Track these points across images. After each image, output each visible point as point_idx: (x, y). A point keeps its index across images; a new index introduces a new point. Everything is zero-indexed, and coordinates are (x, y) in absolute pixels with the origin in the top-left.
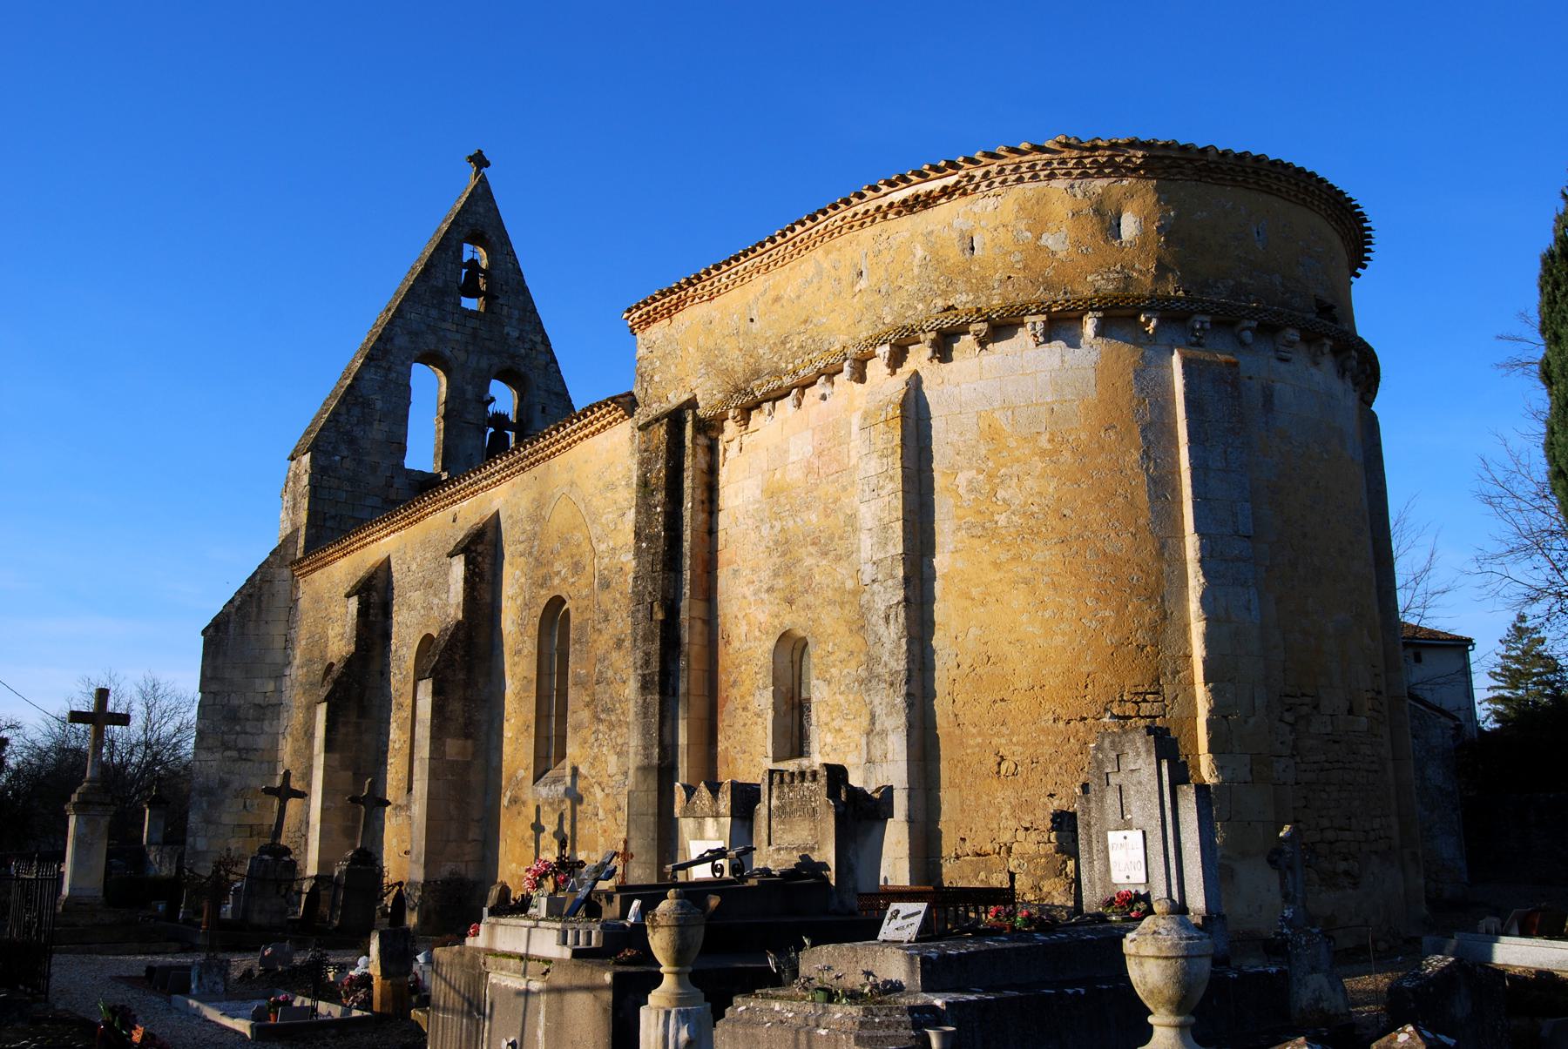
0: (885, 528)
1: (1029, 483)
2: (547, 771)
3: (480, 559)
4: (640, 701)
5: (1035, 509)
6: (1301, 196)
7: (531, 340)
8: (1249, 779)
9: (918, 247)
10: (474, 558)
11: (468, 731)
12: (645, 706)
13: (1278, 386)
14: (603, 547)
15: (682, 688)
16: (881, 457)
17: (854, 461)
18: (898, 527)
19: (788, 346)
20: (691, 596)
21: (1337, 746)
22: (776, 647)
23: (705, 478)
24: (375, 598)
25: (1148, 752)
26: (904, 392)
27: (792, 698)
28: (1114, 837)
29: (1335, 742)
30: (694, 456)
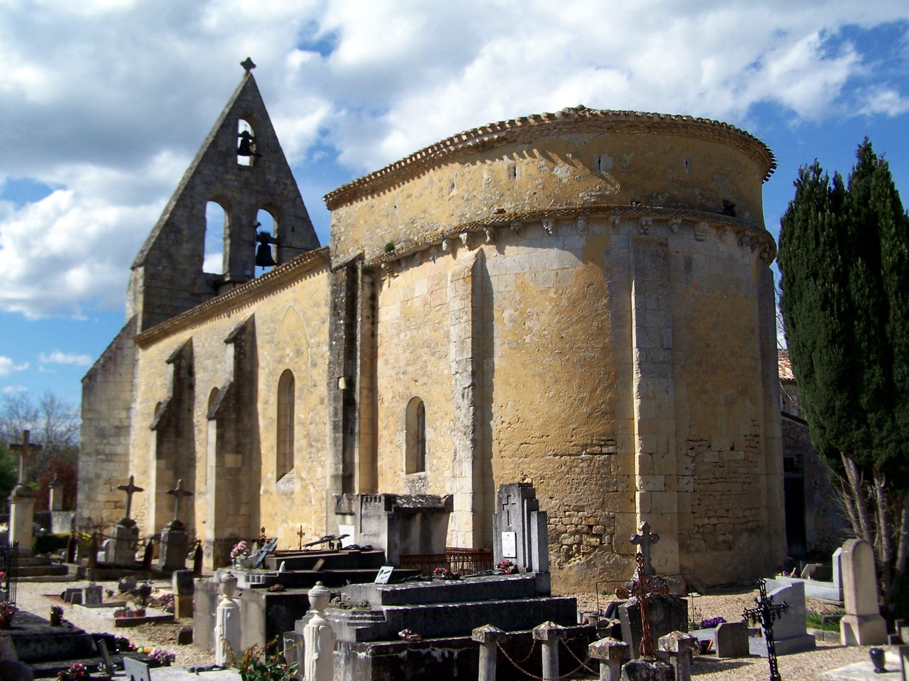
0: (463, 342)
1: (543, 317)
2: (284, 475)
3: (243, 344)
4: (333, 436)
5: (546, 333)
6: (716, 138)
7: (285, 183)
8: (663, 489)
9: (485, 172)
10: (240, 343)
11: (238, 449)
12: (335, 440)
13: (695, 256)
14: (313, 341)
15: (357, 429)
16: (461, 299)
17: (448, 300)
18: (469, 341)
19: (415, 225)
20: (361, 375)
21: (721, 469)
22: (408, 406)
23: (370, 302)
24: (184, 363)
25: (519, 495)
26: (474, 261)
27: (418, 437)
28: (504, 535)
29: (720, 467)
30: (363, 289)
